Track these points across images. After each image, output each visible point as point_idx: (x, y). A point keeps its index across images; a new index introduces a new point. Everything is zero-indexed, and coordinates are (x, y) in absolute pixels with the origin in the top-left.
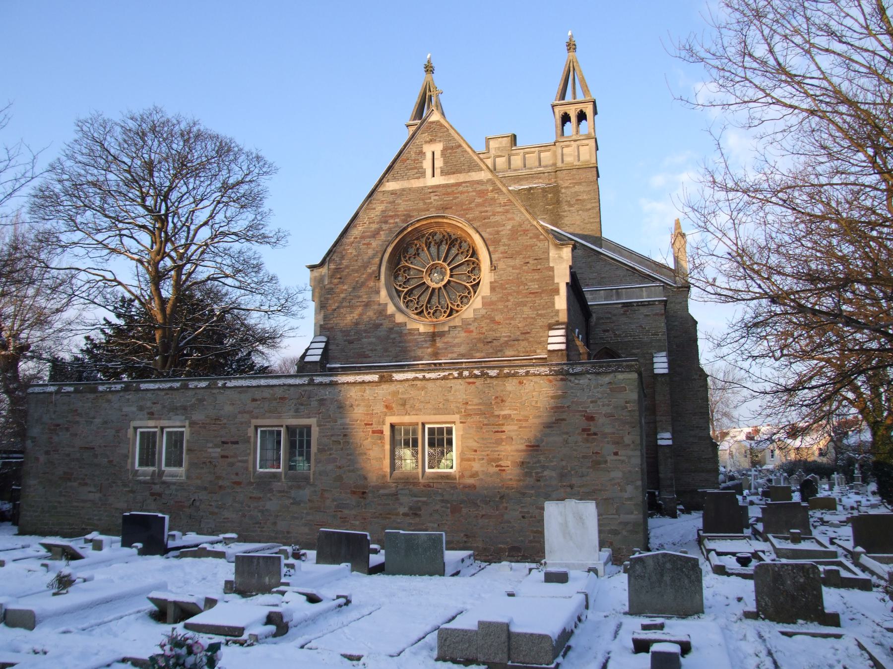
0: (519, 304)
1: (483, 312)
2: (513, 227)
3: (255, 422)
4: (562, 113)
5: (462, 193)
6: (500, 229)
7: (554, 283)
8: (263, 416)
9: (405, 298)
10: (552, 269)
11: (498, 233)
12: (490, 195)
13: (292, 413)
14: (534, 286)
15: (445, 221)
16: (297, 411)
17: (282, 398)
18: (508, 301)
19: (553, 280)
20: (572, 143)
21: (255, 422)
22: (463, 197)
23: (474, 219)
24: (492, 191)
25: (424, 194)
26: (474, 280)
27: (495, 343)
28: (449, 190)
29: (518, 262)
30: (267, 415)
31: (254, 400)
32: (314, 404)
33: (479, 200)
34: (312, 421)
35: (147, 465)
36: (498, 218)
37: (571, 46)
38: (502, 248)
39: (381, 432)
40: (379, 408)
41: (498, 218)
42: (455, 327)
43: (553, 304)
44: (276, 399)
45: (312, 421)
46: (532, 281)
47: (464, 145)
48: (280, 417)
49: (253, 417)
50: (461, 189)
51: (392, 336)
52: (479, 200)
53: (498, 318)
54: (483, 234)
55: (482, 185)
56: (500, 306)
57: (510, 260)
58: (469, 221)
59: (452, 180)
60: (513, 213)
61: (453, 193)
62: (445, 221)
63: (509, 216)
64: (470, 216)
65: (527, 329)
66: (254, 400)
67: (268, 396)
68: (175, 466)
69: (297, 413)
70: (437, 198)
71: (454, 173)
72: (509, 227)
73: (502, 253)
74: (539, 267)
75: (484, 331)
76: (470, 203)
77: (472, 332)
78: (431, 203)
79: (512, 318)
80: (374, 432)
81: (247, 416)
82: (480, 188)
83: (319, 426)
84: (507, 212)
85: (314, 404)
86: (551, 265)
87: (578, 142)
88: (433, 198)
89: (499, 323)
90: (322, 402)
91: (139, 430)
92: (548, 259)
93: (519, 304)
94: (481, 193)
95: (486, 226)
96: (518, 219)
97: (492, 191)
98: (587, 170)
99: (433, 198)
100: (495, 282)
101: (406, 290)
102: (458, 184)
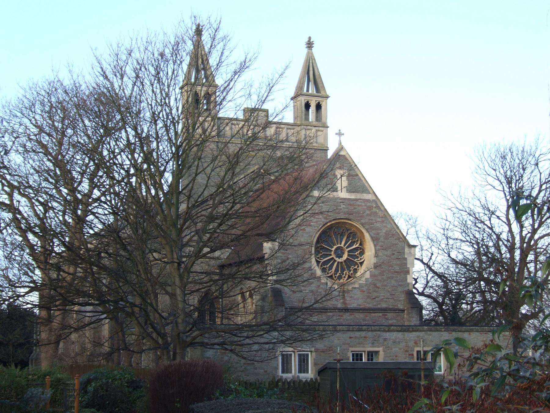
0: (389, 278)
1: (370, 280)
2: (386, 231)
3: (351, 349)
4: (306, 101)
5: (359, 206)
6: (379, 231)
7: (407, 268)
8: (355, 346)
9: (321, 266)
10: (406, 259)
11: (378, 234)
12: (374, 210)
13: (370, 345)
14: (397, 268)
15: (349, 222)
16: (373, 344)
17: (365, 337)
18: (384, 275)
19: (406, 265)
20: (313, 128)
21: (351, 349)
22: (360, 208)
23: (365, 223)
24: (375, 208)
25: (338, 202)
26: (361, 259)
27: (377, 299)
28: (352, 203)
29: (389, 252)
30: (358, 345)
31: (351, 338)
32: (381, 340)
33: (368, 212)
34: (380, 349)
35: (287, 373)
36: (378, 225)
37: (310, 45)
38: (380, 244)
39: (413, 355)
40: (411, 344)
41: (378, 225)
42: (355, 288)
43: (407, 279)
44: (362, 338)
45: (380, 349)
46: (396, 265)
47: (360, 175)
48: (364, 347)
49: (350, 347)
50: (358, 203)
51: (319, 291)
52: (368, 212)
53: (379, 285)
54: (371, 233)
55: (370, 202)
56: (380, 278)
57: (385, 251)
58: (363, 225)
59: (353, 196)
60: (386, 223)
61: (353, 205)
62: (349, 222)
63: (384, 224)
64: (363, 221)
65: (393, 293)
66: (351, 338)
67: (358, 336)
68: (304, 372)
69: (373, 345)
70: (344, 206)
71: (354, 192)
72: (384, 231)
73: (381, 246)
74: (400, 257)
75: (371, 291)
76: (363, 213)
77: (364, 291)
78: (341, 209)
79: (386, 286)
80: (409, 355)
81: (347, 346)
82: (369, 204)
83: (384, 351)
84: (383, 222)
85: (381, 340)
86: (406, 257)
87: (317, 128)
88: (342, 206)
89: (378, 288)
90: (385, 340)
91: (310, 353)
92: (404, 253)
93: (389, 278)
94: (370, 208)
95: (372, 229)
96: (389, 227)
97: (375, 208)
98: (322, 151)
99: (342, 206)
100: (377, 263)
101: (322, 261)
102: (356, 200)
